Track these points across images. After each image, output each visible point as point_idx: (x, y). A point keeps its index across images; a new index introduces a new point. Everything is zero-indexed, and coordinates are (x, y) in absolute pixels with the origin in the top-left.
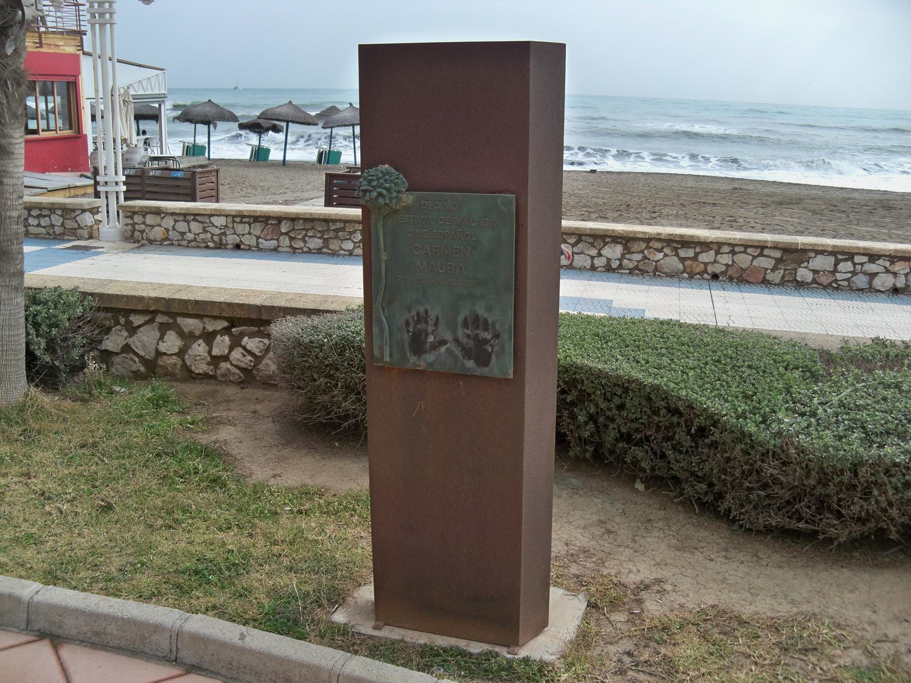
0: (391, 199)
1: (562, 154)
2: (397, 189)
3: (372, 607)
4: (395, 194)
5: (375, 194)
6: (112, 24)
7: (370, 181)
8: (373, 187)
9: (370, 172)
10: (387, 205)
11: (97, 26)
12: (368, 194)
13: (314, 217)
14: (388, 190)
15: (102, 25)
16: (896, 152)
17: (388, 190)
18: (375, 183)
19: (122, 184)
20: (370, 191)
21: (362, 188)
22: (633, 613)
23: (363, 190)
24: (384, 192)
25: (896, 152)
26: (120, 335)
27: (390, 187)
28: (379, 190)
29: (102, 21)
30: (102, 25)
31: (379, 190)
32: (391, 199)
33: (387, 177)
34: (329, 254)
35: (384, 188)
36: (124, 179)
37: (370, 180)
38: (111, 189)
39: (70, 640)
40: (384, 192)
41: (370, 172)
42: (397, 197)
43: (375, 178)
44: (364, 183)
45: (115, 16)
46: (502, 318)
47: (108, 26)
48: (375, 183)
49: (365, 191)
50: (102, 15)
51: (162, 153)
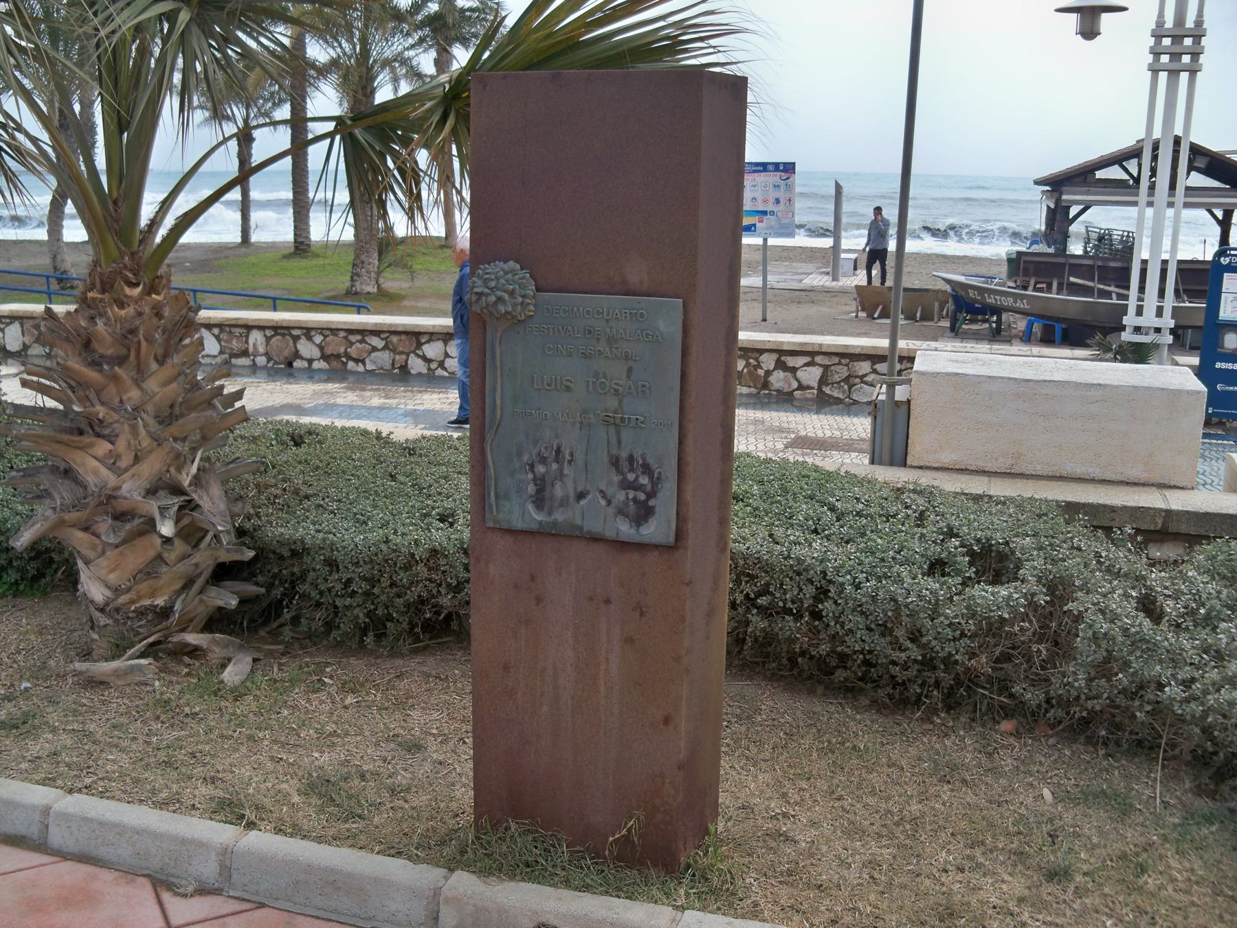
1: (88, 227)
2: (523, 292)
4: (520, 299)
6: (1193, 72)
7: (486, 282)
8: (491, 289)
10: (507, 313)
11: (1163, 76)
12: (484, 298)
13: (852, 351)
14: (512, 293)
15: (1174, 74)
17: (512, 293)
18: (493, 284)
20: (487, 295)
21: (476, 290)
22: (1110, 909)
23: (477, 293)
24: (506, 296)
28: (499, 293)
29: (1175, 66)
30: (1174, 74)
33: (510, 276)
34: (443, 377)
35: (505, 291)
37: (486, 279)
40: (506, 296)
41: (486, 269)
42: (522, 303)
43: (493, 277)
44: (479, 282)
45: (1204, 41)
47: (1184, 76)
49: (480, 294)
50: (1176, 56)
51: (147, 204)
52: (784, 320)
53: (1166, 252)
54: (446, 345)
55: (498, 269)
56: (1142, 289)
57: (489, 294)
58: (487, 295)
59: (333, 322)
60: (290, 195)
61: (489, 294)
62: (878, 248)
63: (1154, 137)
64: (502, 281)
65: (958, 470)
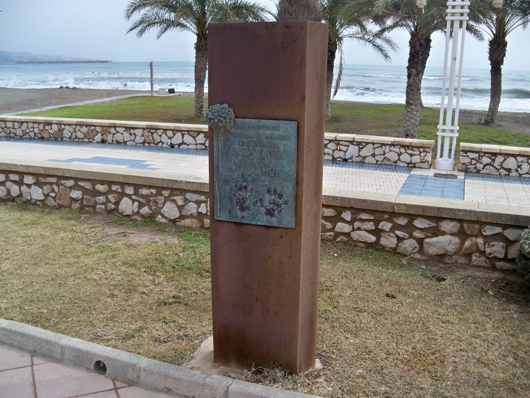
0: (226, 123)
3: (213, 355)
5: (217, 120)
8: (216, 116)
9: (212, 107)
10: (224, 126)
12: (212, 121)
16: (465, 96)
17: (225, 118)
19: (456, 132)
21: (209, 117)
23: (209, 118)
24: (222, 119)
25: (465, 96)
26: (495, 279)
27: (225, 116)
28: (220, 118)
31: (220, 118)
32: (226, 123)
33: (223, 110)
35: (221, 117)
36: (458, 128)
38: (448, 134)
39: (32, 368)
40: (222, 119)
43: (216, 111)
46: (288, 190)
48: (217, 114)
52: (453, 249)
53: (456, 80)
54: (374, 153)
55: (218, 108)
56: (451, 145)
57: (215, 119)
58: (214, 119)
59: (163, 126)
60: (489, 87)
61: (215, 119)
62: (421, 91)
63: (446, 87)
64: (220, 113)
65: (42, 63)
